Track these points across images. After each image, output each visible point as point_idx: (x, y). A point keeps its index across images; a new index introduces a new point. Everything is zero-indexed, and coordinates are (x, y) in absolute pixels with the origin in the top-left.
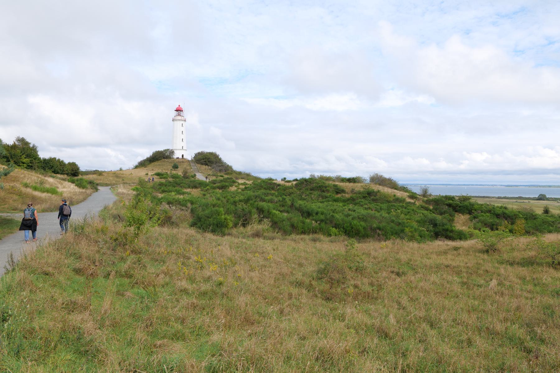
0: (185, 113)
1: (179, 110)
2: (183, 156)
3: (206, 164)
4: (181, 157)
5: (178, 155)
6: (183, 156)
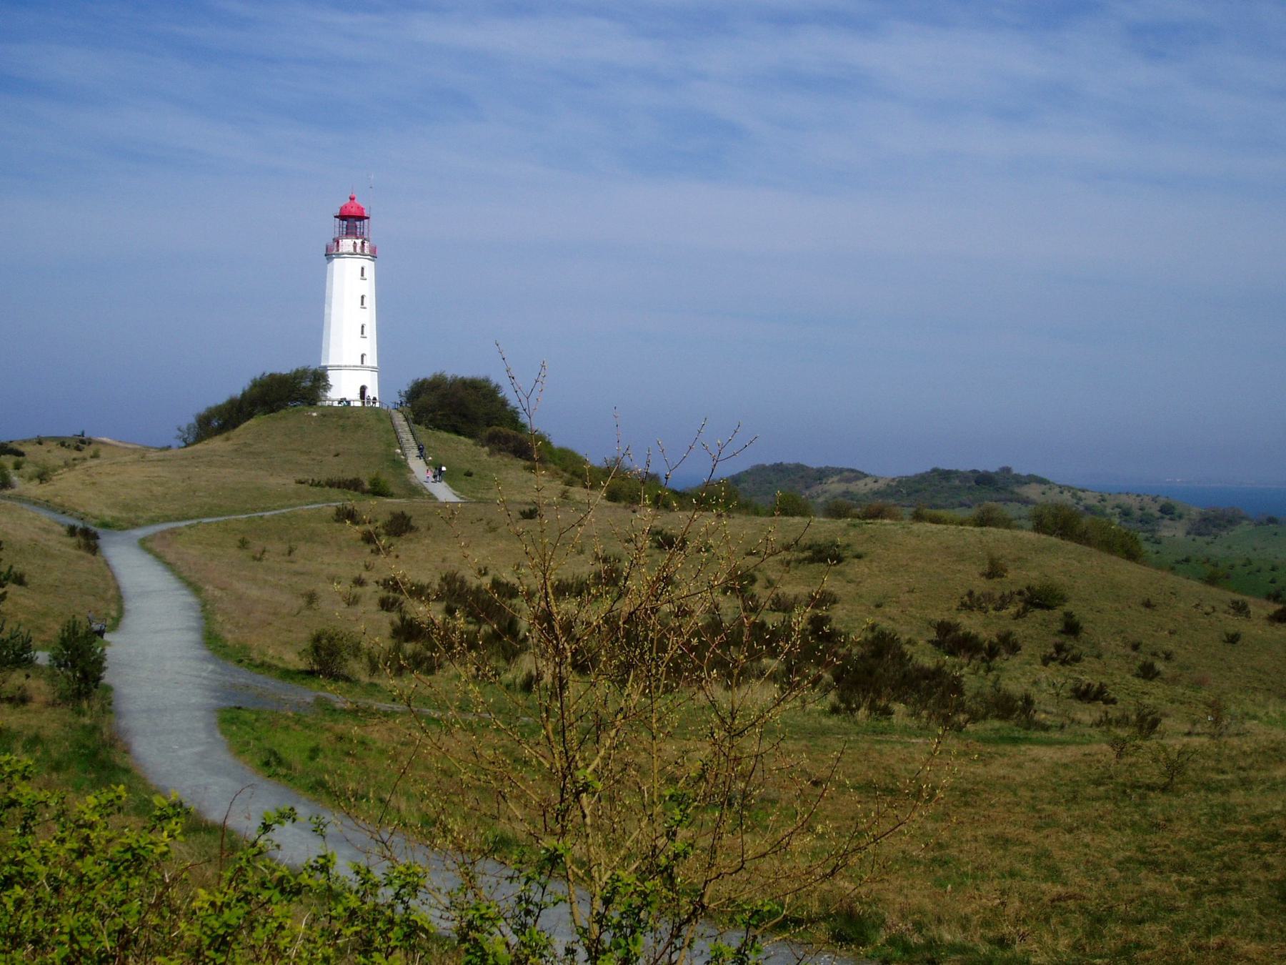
2: (363, 389)
5: (344, 387)
6: (363, 389)
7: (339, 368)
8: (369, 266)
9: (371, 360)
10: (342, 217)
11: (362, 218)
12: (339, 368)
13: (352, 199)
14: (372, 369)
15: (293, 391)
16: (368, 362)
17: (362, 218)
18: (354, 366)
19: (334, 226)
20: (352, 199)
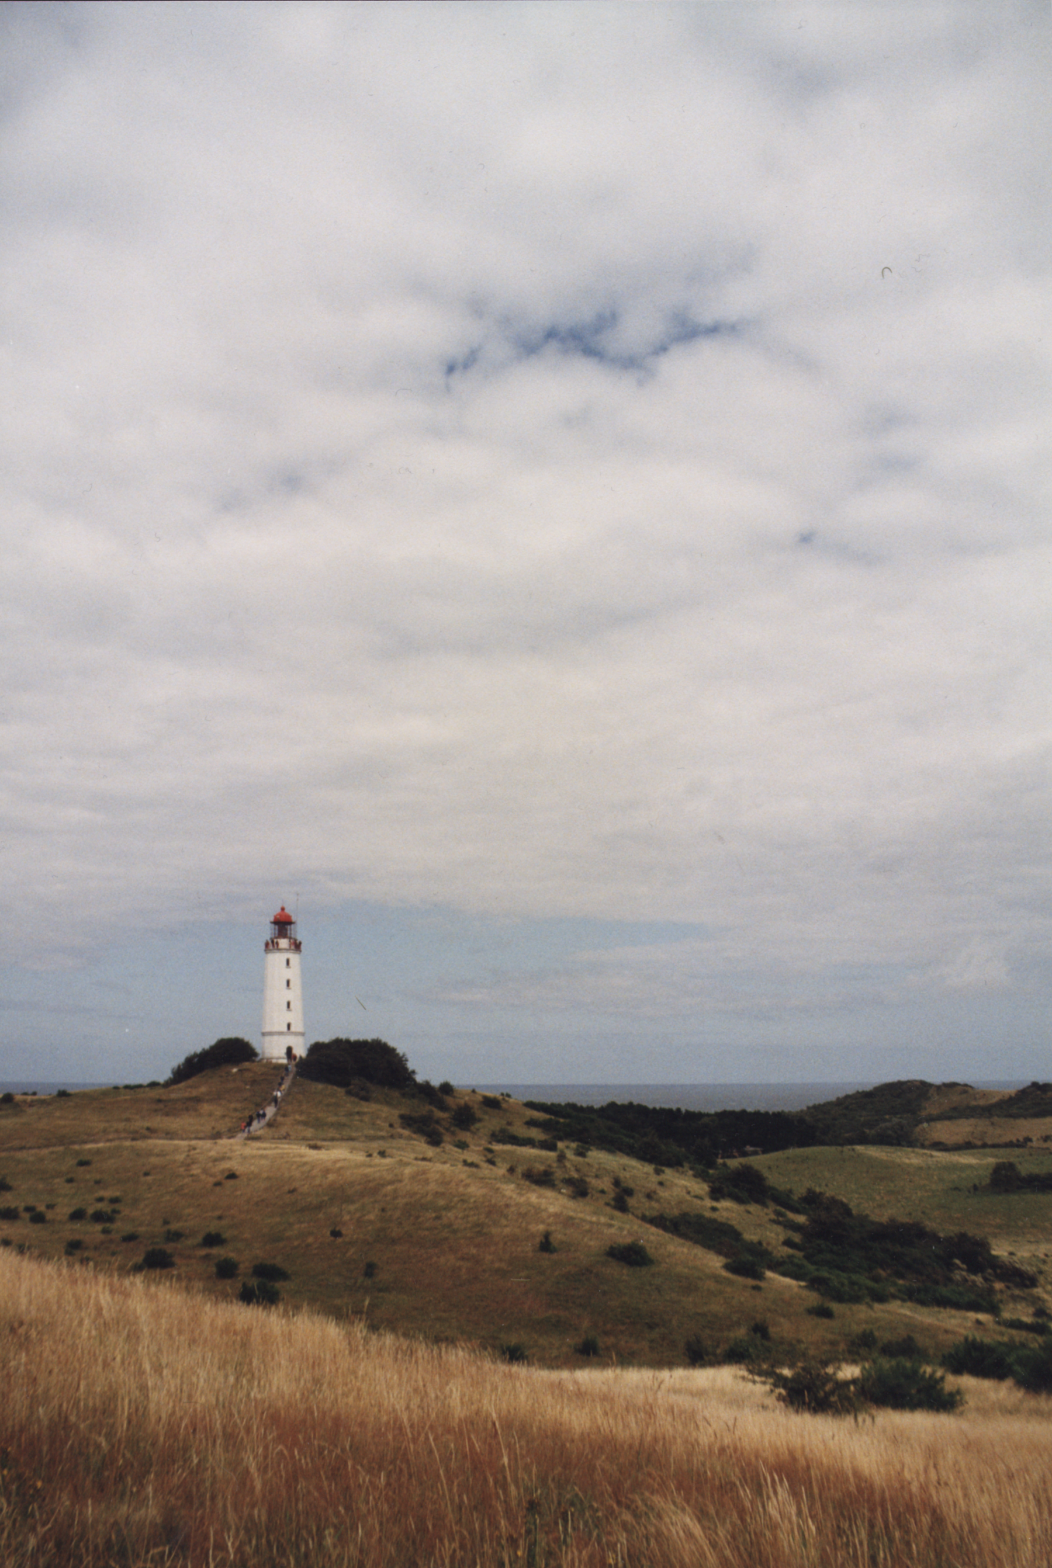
0: (300, 932)
1: (283, 924)
4: (283, 1052)
6: (289, 1050)
7: (271, 1034)
8: (294, 958)
12: (271, 1034)
14: (303, 1034)
16: (293, 1029)
19: (267, 931)
20: (283, 909)
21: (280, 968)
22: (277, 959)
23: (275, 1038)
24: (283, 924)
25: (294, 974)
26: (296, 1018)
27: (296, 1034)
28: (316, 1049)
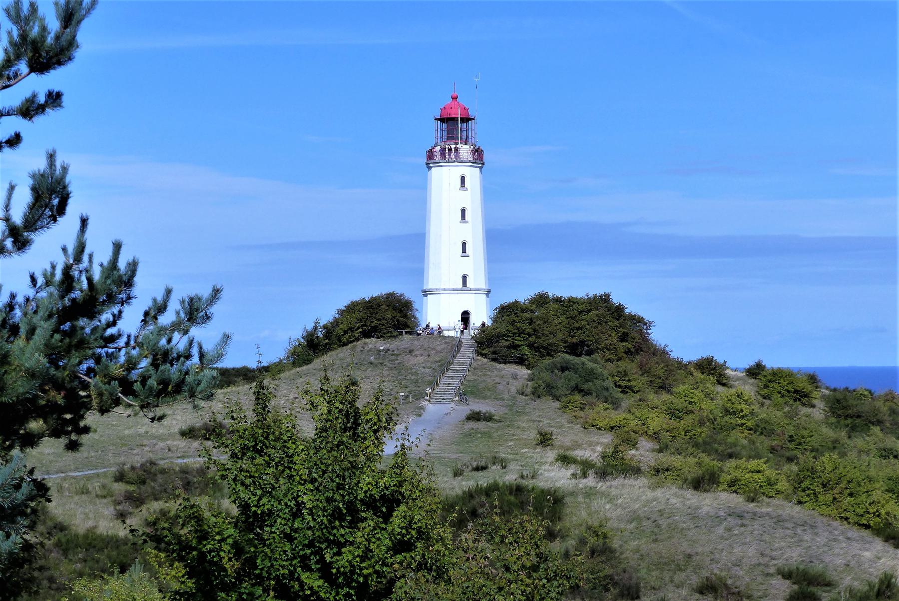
0: (480, 131)
2: (465, 317)
3: (521, 361)
4: (456, 320)
5: (439, 313)
6: (465, 317)
7: (437, 291)
8: (472, 174)
9: (478, 280)
10: (442, 120)
11: (466, 120)
12: (437, 291)
13: (455, 98)
15: (387, 317)
16: (470, 284)
17: (466, 120)
18: (455, 296)
20: (455, 98)
21: (453, 194)
22: (445, 177)
23: (443, 297)
24: (453, 124)
25: (472, 199)
26: (475, 267)
27: (478, 291)
28: (506, 312)
